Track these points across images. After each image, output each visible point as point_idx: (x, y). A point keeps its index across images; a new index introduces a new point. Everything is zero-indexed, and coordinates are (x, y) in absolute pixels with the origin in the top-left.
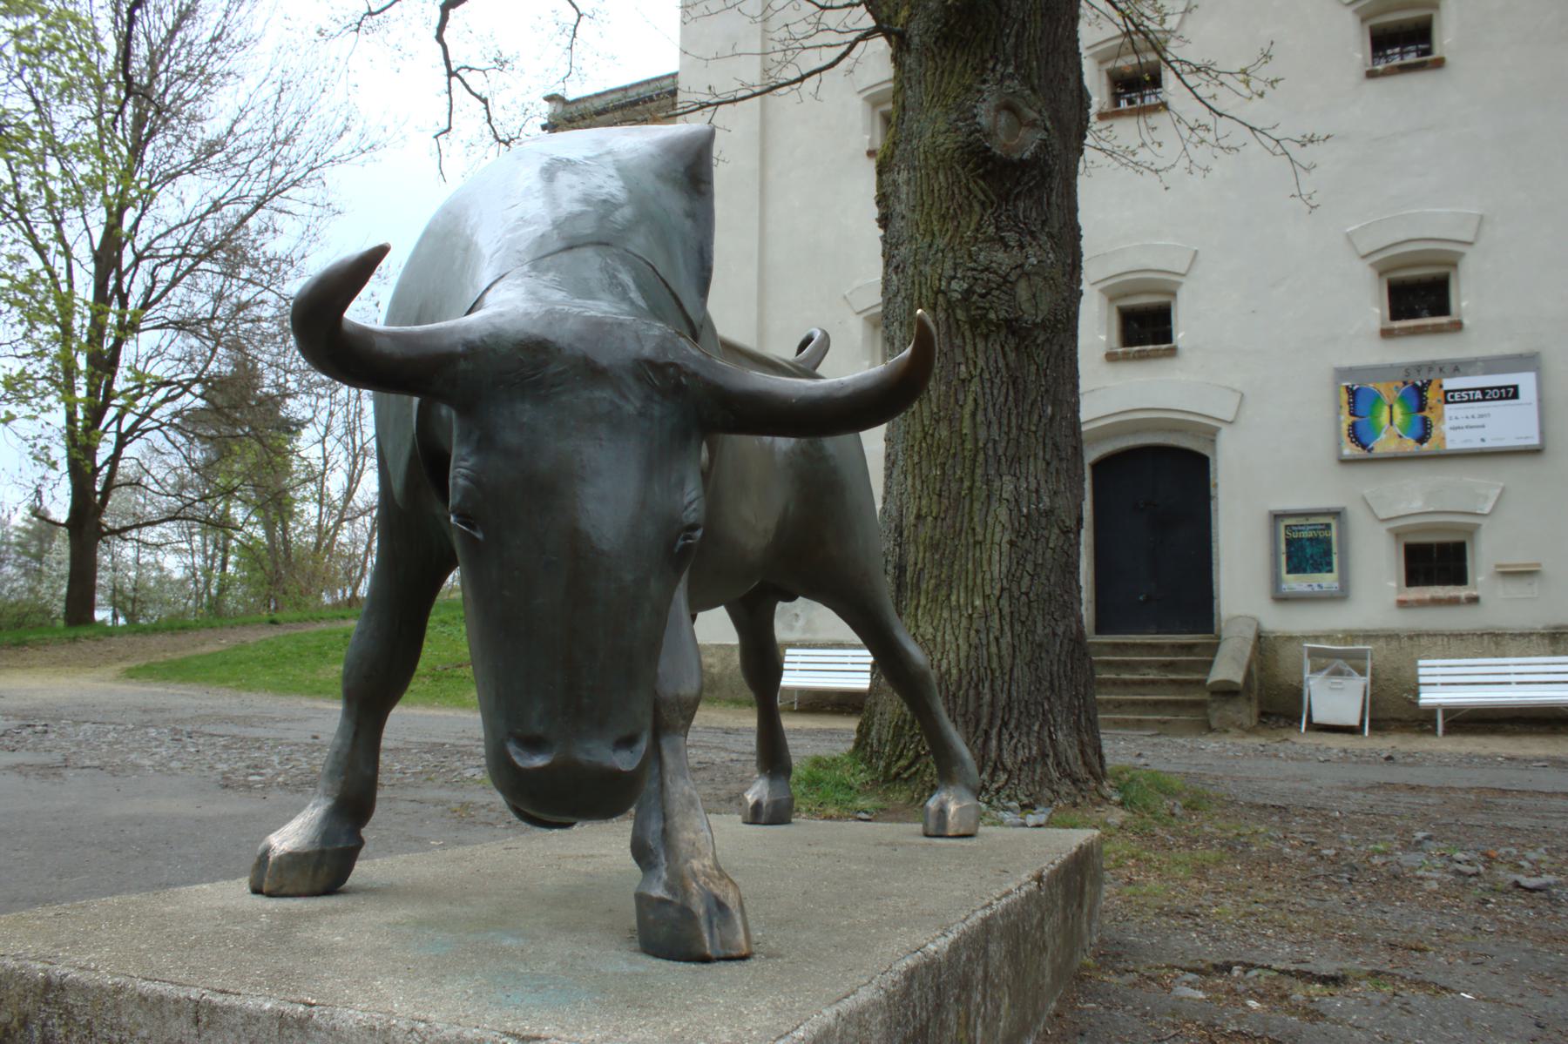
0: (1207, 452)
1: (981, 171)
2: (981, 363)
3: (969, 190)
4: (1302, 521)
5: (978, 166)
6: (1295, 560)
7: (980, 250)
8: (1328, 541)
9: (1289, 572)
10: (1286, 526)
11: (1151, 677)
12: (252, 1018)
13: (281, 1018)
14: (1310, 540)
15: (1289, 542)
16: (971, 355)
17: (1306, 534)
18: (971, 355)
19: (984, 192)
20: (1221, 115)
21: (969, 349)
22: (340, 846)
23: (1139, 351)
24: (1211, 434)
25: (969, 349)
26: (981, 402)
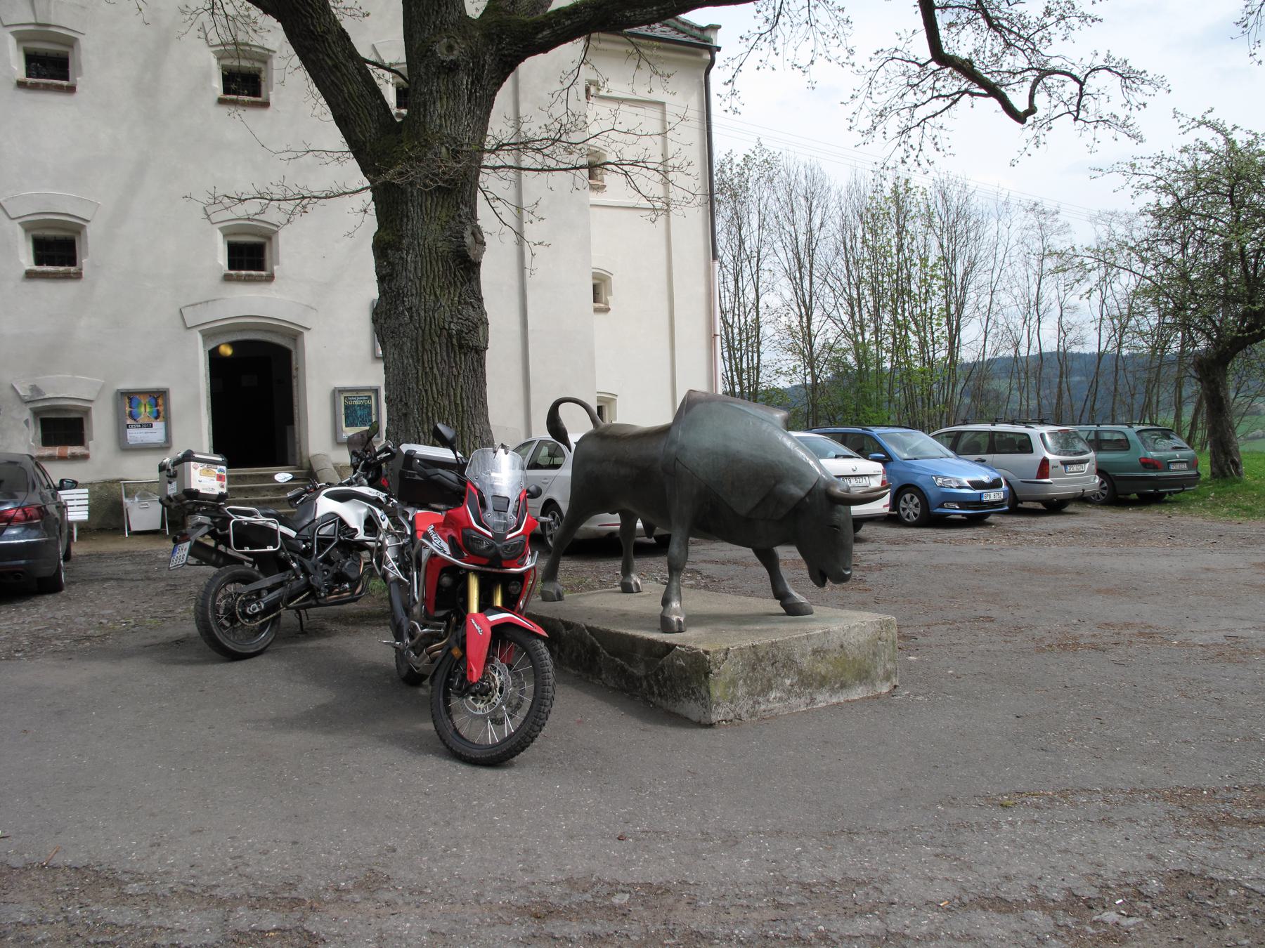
0: (290, 346)
1: (462, 266)
2: (463, 367)
3: (455, 274)
4: (354, 394)
5: (461, 264)
6: (350, 418)
7: (463, 308)
8: (370, 407)
9: (346, 426)
10: (345, 397)
11: (269, 497)
12: (819, 635)
13: (825, 633)
14: (360, 406)
15: (347, 407)
16: (458, 362)
17: (356, 403)
18: (458, 362)
19: (461, 276)
20: (505, 224)
21: (458, 359)
22: (564, 631)
23: (247, 275)
24: (295, 335)
25: (458, 359)
26: (464, 387)
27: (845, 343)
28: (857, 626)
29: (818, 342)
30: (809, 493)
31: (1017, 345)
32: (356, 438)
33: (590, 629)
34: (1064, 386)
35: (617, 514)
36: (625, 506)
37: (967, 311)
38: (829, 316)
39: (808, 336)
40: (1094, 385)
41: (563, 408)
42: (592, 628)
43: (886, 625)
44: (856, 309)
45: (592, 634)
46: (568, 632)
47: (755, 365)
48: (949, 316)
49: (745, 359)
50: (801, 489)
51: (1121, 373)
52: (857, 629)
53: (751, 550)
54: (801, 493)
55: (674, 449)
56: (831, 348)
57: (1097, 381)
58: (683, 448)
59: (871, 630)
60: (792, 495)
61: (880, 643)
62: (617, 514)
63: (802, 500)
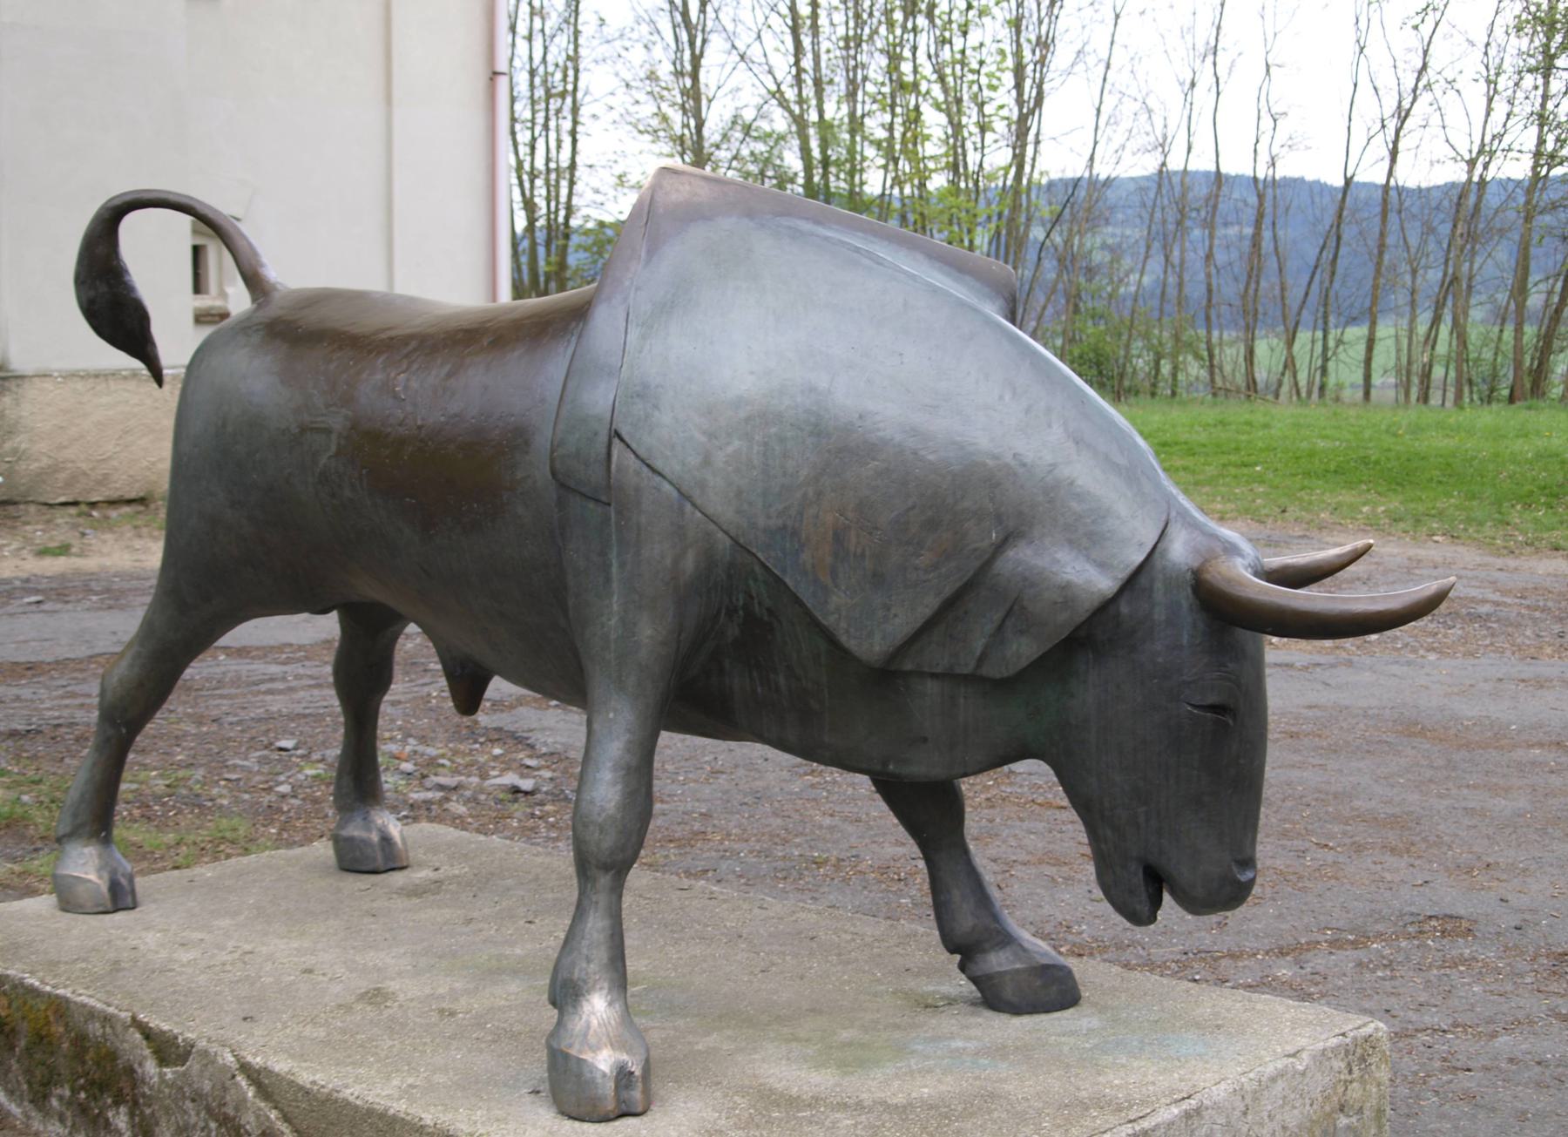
13: (1187, 1115)
22: (151, 1068)
27: (780, 122)
28: (1281, 1074)
29: (715, 120)
30: (1134, 582)
31: (1163, 145)
32: (1435, 194)
33: (256, 1076)
34: (1267, 244)
35: (334, 615)
36: (368, 589)
37: (1060, 58)
38: (742, 57)
39: (693, 100)
40: (1332, 243)
41: (133, 229)
42: (268, 1072)
43: (1359, 1054)
44: (806, 41)
45: (264, 1092)
46: (169, 1073)
47: (565, 163)
48: (1019, 72)
49: (540, 145)
50: (1102, 566)
51: (1393, 218)
52: (1280, 1084)
53: (863, 783)
54: (1104, 584)
55: (598, 398)
56: (747, 130)
57: (1339, 238)
58: (643, 392)
59: (1319, 1082)
60: (1067, 587)
61: (1343, 1121)
62: (334, 615)
63: (1107, 606)
